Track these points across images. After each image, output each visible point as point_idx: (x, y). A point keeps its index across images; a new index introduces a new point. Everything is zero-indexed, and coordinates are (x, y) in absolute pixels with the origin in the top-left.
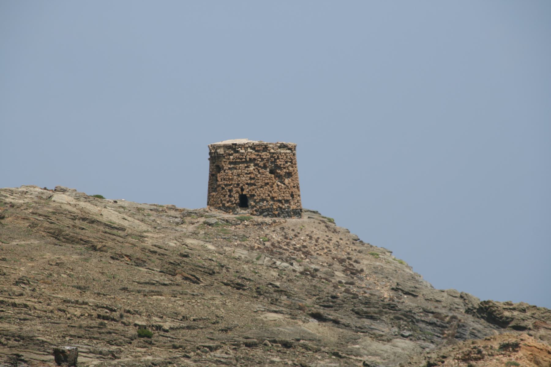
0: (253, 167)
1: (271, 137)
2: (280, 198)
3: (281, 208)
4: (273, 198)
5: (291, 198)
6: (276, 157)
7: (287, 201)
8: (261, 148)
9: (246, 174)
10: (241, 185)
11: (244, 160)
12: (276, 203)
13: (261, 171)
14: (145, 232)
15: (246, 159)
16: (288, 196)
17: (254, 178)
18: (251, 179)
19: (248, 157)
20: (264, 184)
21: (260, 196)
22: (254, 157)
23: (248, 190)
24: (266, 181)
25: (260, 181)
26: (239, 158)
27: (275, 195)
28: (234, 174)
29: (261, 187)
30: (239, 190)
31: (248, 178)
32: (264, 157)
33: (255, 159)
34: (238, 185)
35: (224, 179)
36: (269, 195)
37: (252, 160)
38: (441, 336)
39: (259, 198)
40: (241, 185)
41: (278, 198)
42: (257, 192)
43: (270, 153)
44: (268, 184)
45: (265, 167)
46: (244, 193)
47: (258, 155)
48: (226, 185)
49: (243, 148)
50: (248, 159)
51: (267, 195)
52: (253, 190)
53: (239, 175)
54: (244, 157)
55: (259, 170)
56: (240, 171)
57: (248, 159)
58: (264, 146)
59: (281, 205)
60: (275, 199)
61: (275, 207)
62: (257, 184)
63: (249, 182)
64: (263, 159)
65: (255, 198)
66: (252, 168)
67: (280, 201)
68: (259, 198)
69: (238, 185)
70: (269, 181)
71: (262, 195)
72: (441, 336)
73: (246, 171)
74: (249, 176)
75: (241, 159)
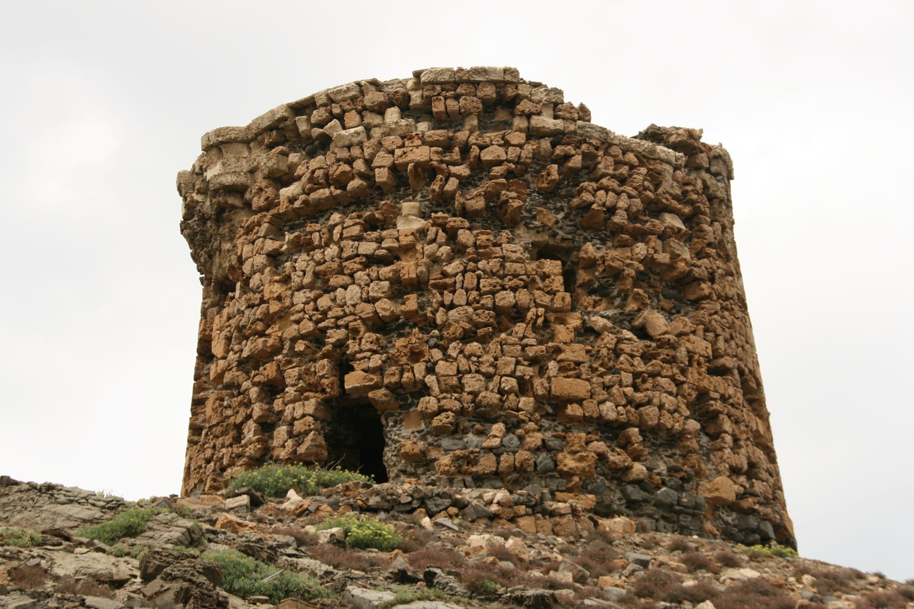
0: (418, 224)
1: (513, 67)
2: (609, 411)
3: (619, 474)
4: (554, 407)
5: (693, 425)
6: (576, 161)
7: (664, 439)
8: (470, 102)
9: (371, 261)
10: (334, 336)
11: (355, 183)
12: (578, 436)
13: (465, 236)
14: (664, 334)
15: (368, 177)
16: (666, 406)
17: (419, 285)
18: (399, 288)
19: (383, 159)
20: (484, 317)
21: (459, 388)
22: (421, 154)
23: (376, 361)
24: (506, 298)
25: (460, 297)
26: (328, 181)
27: (565, 386)
29: (466, 337)
30: (323, 366)
31: (379, 288)
32: (487, 155)
33: (427, 171)
36: (524, 387)
37: (404, 180)
38: (107, 548)
39: (451, 403)
40: (334, 336)
41: (590, 408)
42: (442, 367)
43: (533, 134)
44: (517, 313)
45: (497, 216)
46: (353, 381)
47: (447, 146)
49: (352, 118)
50: (382, 176)
51: (510, 383)
52: (415, 355)
53: (321, 282)
54: (359, 165)
55: (452, 235)
56: (332, 251)
57: (382, 176)
58: (489, 91)
59: (617, 457)
60: (573, 410)
61: (569, 462)
62: (440, 318)
63: (385, 307)
64: (481, 168)
65: (429, 403)
66: (409, 221)
67: (612, 431)
68: (451, 403)
69: (317, 338)
70: (523, 297)
71: (472, 382)
72: (107, 548)
73: (367, 248)
74: (386, 271)
75: (341, 182)
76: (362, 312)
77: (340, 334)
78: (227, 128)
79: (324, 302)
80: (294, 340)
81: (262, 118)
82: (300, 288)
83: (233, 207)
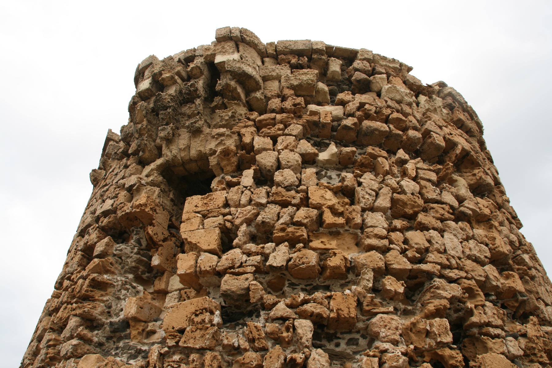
28: (364, 195)
34: (417, 283)
35: (263, 234)
48: (278, 279)
76: (473, 271)
77: (455, 290)
78: (252, 33)
79: (417, 238)
80: (381, 273)
81: (296, 42)
82: (372, 209)
83: (239, 99)
